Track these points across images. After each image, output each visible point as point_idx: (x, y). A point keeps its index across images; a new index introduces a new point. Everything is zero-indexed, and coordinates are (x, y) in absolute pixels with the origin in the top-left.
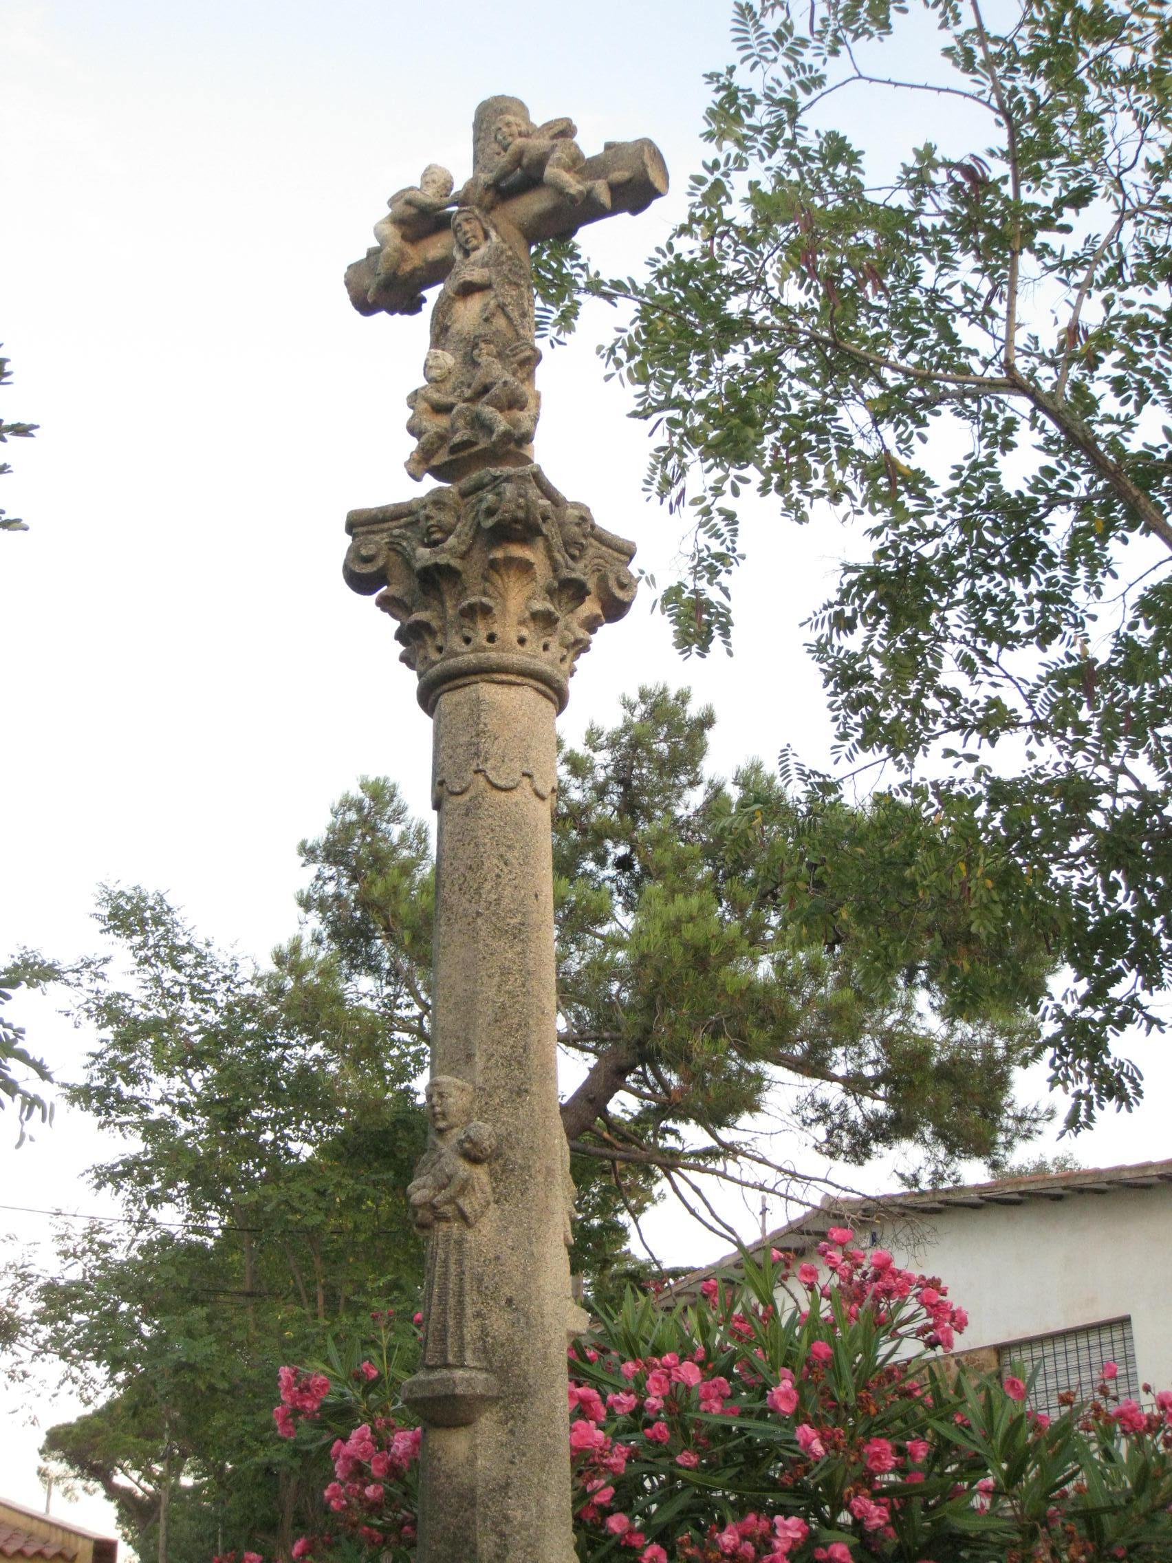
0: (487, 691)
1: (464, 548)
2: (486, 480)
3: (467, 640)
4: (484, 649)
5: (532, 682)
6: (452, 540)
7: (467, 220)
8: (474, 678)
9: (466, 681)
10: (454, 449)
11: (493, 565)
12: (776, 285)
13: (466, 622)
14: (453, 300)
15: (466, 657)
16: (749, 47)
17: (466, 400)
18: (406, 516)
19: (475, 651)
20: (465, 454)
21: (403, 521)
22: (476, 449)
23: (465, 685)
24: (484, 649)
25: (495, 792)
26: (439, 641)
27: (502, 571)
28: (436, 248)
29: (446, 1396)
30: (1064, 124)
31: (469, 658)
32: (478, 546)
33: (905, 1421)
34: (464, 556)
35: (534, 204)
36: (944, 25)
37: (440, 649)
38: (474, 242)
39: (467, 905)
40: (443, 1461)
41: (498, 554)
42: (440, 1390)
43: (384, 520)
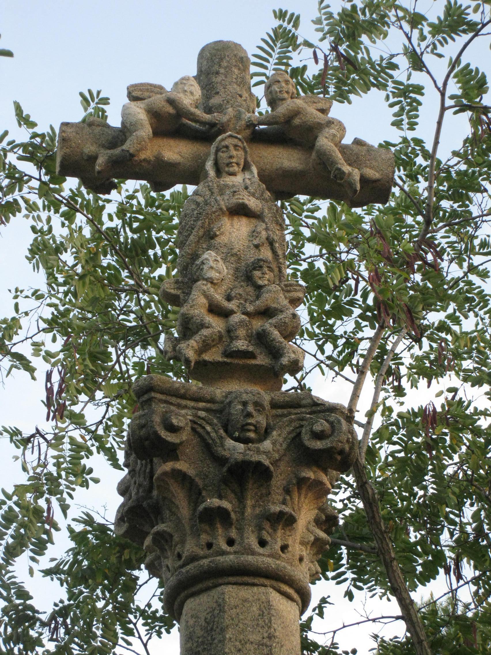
0: (232, 593)
1: (277, 456)
2: (304, 402)
3: (263, 543)
4: (224, 553)
5: (182, 595)
6: (267, 445)
7: (236, 146)
8: (267, 582)
9: (256, 581)
10: (228, 354)
11: (301, 482)
13: (267, 525)
14: (223, 213)
15: (260, 559)
16: (266, 68)
18: (208, 401)
19: (270, 556)
20: (241, 362)
21: (201, 405)
22: (253, 362)
23: (254, 585)
24: (224, 553)
26: (233, 533)
27: (303, 492)
28: (175, 151)
31: (262, 559)
32: (286, 459)
34: (275, 463)
35: (286, 159)
36: (397, 124)
37: (231, 542)
38: (236, 168)
41: (310, 474)
43: (183, 397)
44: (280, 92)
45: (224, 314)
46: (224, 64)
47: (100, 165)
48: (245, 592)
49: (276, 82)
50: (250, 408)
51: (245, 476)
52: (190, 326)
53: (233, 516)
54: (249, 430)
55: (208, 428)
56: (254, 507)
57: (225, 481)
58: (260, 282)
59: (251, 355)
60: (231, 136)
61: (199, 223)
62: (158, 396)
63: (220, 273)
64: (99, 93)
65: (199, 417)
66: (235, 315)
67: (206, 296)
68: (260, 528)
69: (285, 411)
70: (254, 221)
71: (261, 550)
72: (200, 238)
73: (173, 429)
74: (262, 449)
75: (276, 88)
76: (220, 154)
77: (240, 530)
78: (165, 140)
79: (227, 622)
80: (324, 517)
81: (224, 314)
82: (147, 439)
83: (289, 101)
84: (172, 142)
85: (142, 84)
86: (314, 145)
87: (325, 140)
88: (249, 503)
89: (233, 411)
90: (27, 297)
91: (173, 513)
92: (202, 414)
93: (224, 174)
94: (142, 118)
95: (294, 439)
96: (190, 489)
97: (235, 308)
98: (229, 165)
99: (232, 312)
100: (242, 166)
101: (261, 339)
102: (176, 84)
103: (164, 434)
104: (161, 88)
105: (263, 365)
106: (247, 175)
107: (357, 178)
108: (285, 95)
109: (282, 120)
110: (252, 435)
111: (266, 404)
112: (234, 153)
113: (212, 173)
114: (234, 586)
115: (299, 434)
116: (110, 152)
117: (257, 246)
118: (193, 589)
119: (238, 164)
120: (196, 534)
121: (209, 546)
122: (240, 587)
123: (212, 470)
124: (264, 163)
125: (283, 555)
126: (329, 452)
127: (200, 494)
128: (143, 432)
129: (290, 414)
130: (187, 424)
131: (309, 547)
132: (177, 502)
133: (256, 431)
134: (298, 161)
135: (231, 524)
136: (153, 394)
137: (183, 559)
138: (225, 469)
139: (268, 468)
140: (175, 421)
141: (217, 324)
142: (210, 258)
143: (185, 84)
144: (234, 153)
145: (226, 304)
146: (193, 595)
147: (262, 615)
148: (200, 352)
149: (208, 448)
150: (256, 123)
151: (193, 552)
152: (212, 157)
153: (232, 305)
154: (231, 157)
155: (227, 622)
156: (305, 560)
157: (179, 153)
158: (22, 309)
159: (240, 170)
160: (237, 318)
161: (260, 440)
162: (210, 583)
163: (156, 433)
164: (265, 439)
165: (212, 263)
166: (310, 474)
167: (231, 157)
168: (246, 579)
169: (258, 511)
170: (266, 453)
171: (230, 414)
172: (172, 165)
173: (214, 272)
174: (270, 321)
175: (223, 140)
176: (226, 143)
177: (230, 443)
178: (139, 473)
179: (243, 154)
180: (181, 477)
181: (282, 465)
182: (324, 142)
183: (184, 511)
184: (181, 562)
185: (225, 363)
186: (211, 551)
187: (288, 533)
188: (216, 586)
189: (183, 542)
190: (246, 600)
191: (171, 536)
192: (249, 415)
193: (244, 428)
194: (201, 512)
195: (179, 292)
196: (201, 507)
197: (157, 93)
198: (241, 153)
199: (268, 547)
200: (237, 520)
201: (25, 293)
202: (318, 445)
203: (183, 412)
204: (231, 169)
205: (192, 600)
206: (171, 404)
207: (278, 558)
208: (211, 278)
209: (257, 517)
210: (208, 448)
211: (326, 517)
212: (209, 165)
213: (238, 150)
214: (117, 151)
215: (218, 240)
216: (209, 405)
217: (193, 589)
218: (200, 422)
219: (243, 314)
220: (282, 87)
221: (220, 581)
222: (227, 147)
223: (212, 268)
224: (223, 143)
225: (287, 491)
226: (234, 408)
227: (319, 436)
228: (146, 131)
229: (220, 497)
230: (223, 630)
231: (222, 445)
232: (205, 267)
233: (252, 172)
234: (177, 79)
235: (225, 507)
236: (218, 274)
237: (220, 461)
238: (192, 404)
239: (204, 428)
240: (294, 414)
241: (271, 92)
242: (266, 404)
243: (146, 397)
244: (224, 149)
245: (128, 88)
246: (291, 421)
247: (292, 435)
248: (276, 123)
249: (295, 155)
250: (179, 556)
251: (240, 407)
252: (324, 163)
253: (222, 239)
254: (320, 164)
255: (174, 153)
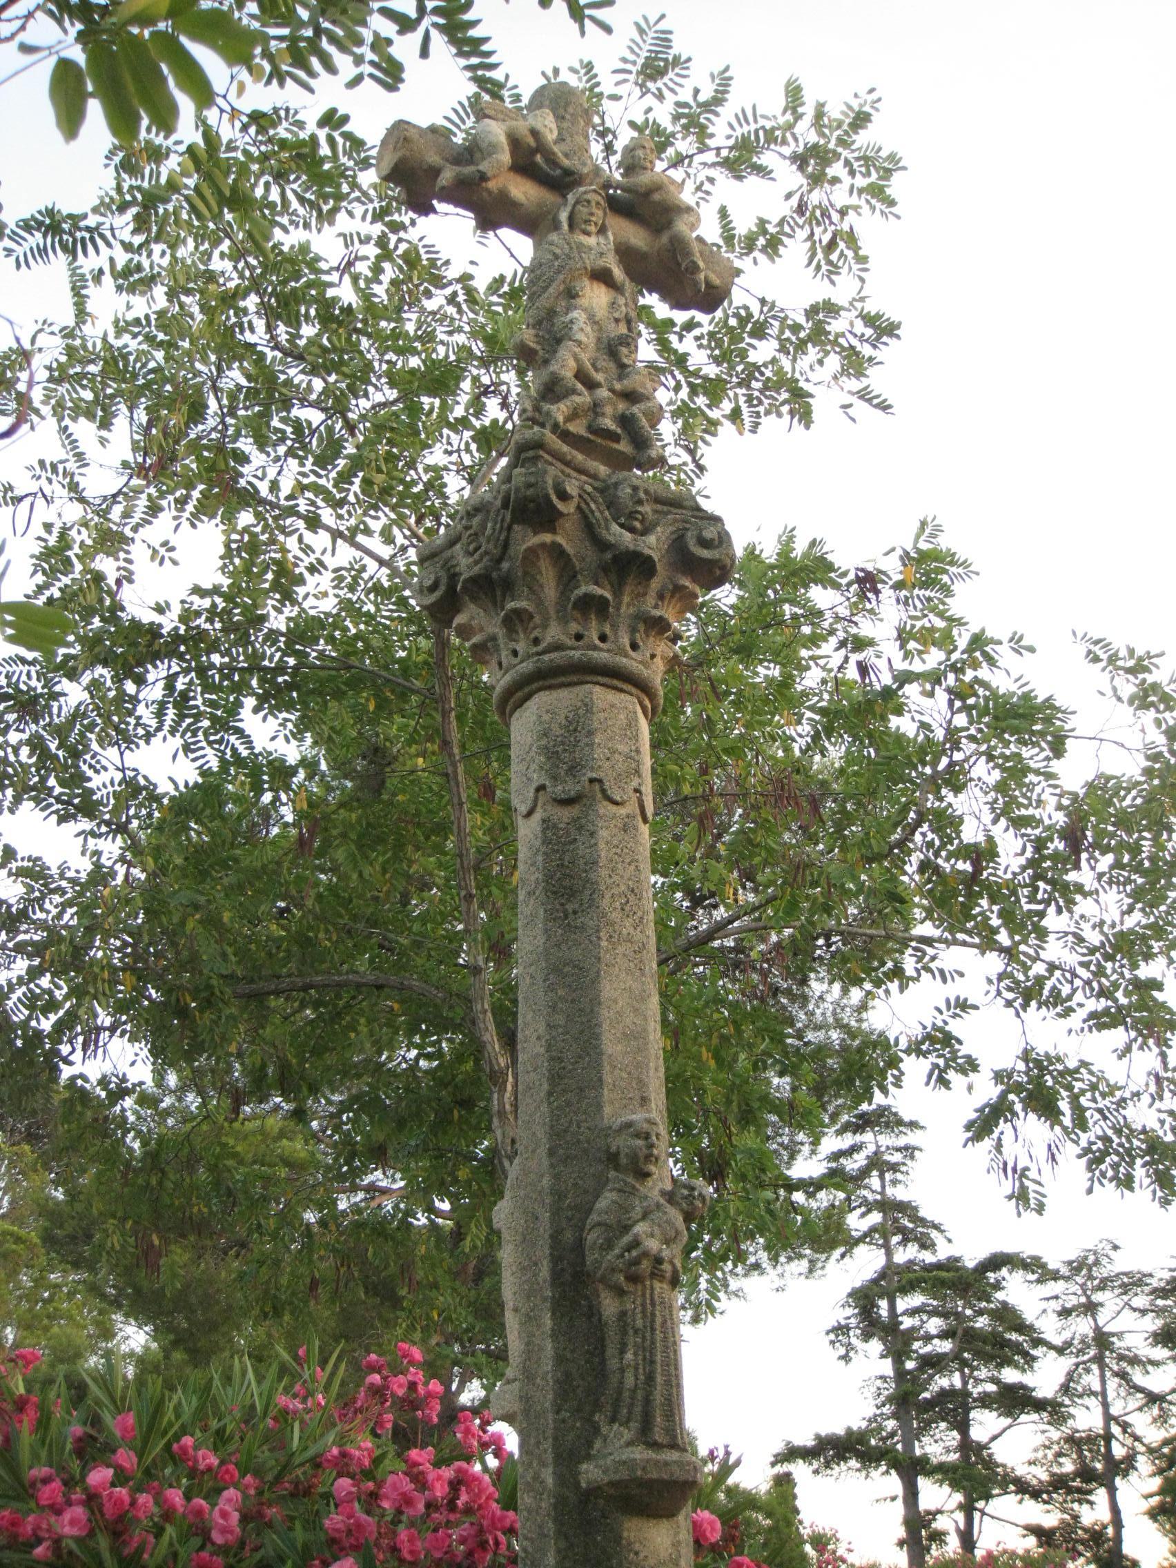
0: (601, 696)
2: (687, 503)
3: (634, 647)
4: (595, 648)
5: (534, 686)
8: (634, 690)
11: (678, 589)
12: (686, 457)
13: (641, 627)
17: (612, 390)
22: (615, 446)
23: (622, 691)
24: (595, 648)
25: (606, 803)
26: (607, 630)
28: (523, 191)
29: (686, 1483)
30: (476, 379)
31: (632, 663)
33: (62, 1361)
37: (603, 638)
38: (593, 229)
39: (631, 930)
40: (642, 1555)
42: (678, 1474)
45: (591, 385)
46: (571, 110)
48: (612, 697)
51: (629, 567)
55: (593, 506)
56: (628, 605)
57: (605, 569)
58: (625, 361)
59: (615, 438)
61: (561, 277)
62: (547, 457)
64: (296, 112)
67: (577, 359)
68: (633, 630)
69: (665, 508)
70: (612, 293)
73: (564, 496)
76: (579, 207)
77: (614, 627)
79: (596, 725)
81: (591, 385)
82: (532, 501)
88: (626, 599)
89: (620, 494)
90: (52, 333)
95: (674, 541)
98: (587, 222)
99: (598, 385)
101: (626, 421)
106: (602, 240)
109: (642, 190)
110: (637, 525)
113: (565, 226)
116: (458, 169)
117: (617, 321)
118: (547, 683)
120: (564, 620)
121: (579, 637)
123: (591, 555)
126: (711, 563)
127: (575, 577)
128: (530, 492)
129: (669, 513)
132: (543, 580)
133: (642, 522)
136: (541, 453)
144: (594, 210)
146: (550, 687)
147: (630, 725)
148: (568, 419)
149: (589, 529)
152: (569, 208)
153: (599, 377)
154: (592, 214)
155: (596, 725)
157: (525, 193)
158: (37, 345)
160: (603, 393)
162: (575, 678)
163: (547, 497)
166: (686, 582)
167: (592, 214)
168: (616, 682)
169: (631, 610)
172: (515, 204)
176: (588, 197)
177: (615, 528)
180: (557, 553)
183: (550, 592)
185: (589, 441)
188: (582, 683)
189: (545, 626)
190: (613, 706)
191: (531, 617)
195: (538, 347)
198: (600, 213)
201: (53, 328)
202: (705, 554)
209: (630, 616)
210: (589, 529)
214: (468, 170)
215: (579, 301)
217: (547, 683)
222: (589, 202)
225: (661, 597)
229: (597, 583)
230: (590, 733)
231: (608, 529)
232: (575, 327)
233: (607, 238)
237: (601, 545)
240: (677, 514)
243: (531, 453)
246: (675, 521)
248: (636, 192)
251: (629, 491)
253: (583, 302)
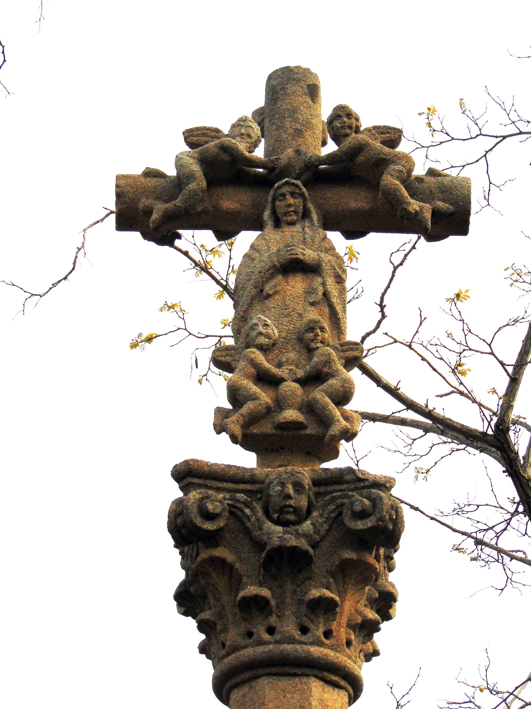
3: (304, 630)
5: (228, 685)
6: (307, 526)
21: (241, 486)
23: (295, 675)
26: (273, 620)
37: (271, 631)
44: (342, 127)
47: (154, 222)
49: (337, 117)
50: (290, 490)
52: (238, 398)
53: (273, 602)
54: (288, 513)
60: (287, 183)
63: (270, 338)
65: (238, 501)
66: (285, 383)
71: (303, 638)
72: (253, 298)
73: (209, 516)
74: (300, 531)
75: (337, 124)
78: (224, 188)
80: (377, 595)
83: (354, 135)
84: (230, 190)
85: (197, 129)
86: (378, 184)
87: (390, 178)
89: (272, 493)
91: (218, 600)
92: (241, 496)
93: (283, 224)
94: (195, 169)
96: (230, 576)
97: (285, 375)
100: (301, 214)
101: (310, 408)
102: (233, 126)
103: (198, 521)
104: (217, 131)
105: (314, 435)
107: (428, 215)
108: (348, 131)
110: (291, 517)
111: (307, 482)
112: (292, 201)
114: (275, 677)
115: (340, 514)
119: (295, 212)
122: (281, 678)
124: (329, 205)
125: (327, 642)
130: (223, 510)
131: (357, 630)
134: (365, 200)
135: (270, 613)
137: (227, 648)
138: (264, 555)
139: (307, 552)
140: (210, 507)
141: (265, 397)
142: (259, 323)
143: (241, 125)
145: (274, 370)
146: (236, 686)
150: (317, 163)
151: (234, 641)
152: (269, 206)
156: (354, 643)
159: (300, 218)
161: (300, 521)
163: (191, 522)
164: (306, 518)
165: (261, 329)
170: (305, 535)
171: (269, 496)
173: (263, 338)
174: (321, 387)
175: (279, 187)
177: (268, 525)
178: (187, 555)
179: (301, 201)
181: (325, 546)
182: (390, 180)
184: (224, 652)
186: (251, 641)
187: (331, 618)
191: (215, 624)
192: (288, 497)
193: (282, 510)
194: (239, 601)
196: (242, 594)
197: (213, 137)
199: (309, 635)
200: (277, 607)
202: (360, 525)
203: (221, 496)
204: (289, 219)
205: (236, 691)
206: (210, 488)
207: (321, 644)
208: (261, 344)
211: (380, 593)
212: (267, 214)
213: (295, 198)
216: (248, 487)
218: (240, 505)
219: (293, 381)
220: (345, 122)
221: (261, 672)
222: (284, 195)
223: (261, 334)
224: (279, 192)
226: (273, 489)
227: (363, 515)
228: (200, 182)
231: (260, 529)
234: (234, 121)
235: (262, 595)
236: (267, 340)
238: (230, 485)
239: (242, 511)
241: (333, 128)
242: (307, 482)
244: (282, 198)
245: (183, 134)
246: (333, 499)
247: (333, 515)
249: (362, 193)
250: (223, 645)
252: (391, 202)
254: (386, 202)
255: (234, 201)
